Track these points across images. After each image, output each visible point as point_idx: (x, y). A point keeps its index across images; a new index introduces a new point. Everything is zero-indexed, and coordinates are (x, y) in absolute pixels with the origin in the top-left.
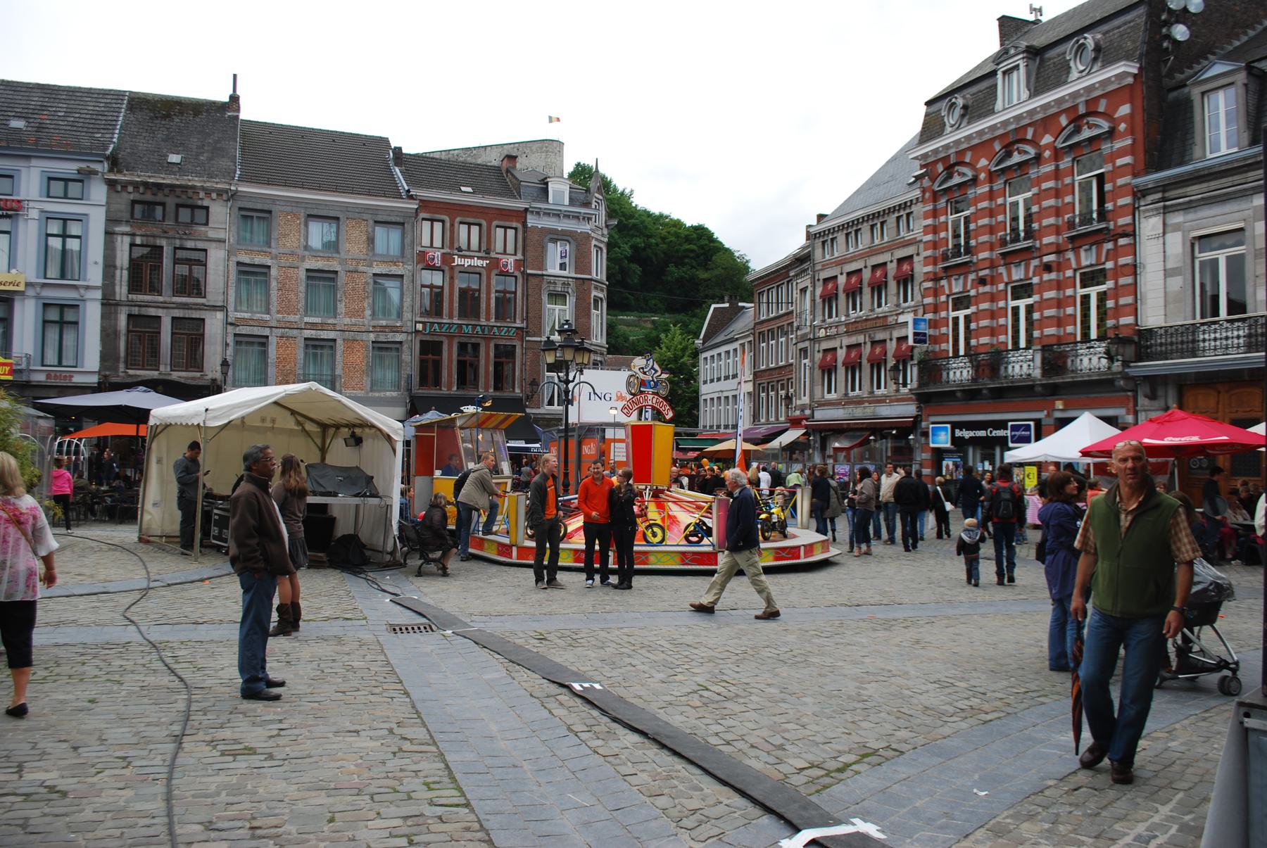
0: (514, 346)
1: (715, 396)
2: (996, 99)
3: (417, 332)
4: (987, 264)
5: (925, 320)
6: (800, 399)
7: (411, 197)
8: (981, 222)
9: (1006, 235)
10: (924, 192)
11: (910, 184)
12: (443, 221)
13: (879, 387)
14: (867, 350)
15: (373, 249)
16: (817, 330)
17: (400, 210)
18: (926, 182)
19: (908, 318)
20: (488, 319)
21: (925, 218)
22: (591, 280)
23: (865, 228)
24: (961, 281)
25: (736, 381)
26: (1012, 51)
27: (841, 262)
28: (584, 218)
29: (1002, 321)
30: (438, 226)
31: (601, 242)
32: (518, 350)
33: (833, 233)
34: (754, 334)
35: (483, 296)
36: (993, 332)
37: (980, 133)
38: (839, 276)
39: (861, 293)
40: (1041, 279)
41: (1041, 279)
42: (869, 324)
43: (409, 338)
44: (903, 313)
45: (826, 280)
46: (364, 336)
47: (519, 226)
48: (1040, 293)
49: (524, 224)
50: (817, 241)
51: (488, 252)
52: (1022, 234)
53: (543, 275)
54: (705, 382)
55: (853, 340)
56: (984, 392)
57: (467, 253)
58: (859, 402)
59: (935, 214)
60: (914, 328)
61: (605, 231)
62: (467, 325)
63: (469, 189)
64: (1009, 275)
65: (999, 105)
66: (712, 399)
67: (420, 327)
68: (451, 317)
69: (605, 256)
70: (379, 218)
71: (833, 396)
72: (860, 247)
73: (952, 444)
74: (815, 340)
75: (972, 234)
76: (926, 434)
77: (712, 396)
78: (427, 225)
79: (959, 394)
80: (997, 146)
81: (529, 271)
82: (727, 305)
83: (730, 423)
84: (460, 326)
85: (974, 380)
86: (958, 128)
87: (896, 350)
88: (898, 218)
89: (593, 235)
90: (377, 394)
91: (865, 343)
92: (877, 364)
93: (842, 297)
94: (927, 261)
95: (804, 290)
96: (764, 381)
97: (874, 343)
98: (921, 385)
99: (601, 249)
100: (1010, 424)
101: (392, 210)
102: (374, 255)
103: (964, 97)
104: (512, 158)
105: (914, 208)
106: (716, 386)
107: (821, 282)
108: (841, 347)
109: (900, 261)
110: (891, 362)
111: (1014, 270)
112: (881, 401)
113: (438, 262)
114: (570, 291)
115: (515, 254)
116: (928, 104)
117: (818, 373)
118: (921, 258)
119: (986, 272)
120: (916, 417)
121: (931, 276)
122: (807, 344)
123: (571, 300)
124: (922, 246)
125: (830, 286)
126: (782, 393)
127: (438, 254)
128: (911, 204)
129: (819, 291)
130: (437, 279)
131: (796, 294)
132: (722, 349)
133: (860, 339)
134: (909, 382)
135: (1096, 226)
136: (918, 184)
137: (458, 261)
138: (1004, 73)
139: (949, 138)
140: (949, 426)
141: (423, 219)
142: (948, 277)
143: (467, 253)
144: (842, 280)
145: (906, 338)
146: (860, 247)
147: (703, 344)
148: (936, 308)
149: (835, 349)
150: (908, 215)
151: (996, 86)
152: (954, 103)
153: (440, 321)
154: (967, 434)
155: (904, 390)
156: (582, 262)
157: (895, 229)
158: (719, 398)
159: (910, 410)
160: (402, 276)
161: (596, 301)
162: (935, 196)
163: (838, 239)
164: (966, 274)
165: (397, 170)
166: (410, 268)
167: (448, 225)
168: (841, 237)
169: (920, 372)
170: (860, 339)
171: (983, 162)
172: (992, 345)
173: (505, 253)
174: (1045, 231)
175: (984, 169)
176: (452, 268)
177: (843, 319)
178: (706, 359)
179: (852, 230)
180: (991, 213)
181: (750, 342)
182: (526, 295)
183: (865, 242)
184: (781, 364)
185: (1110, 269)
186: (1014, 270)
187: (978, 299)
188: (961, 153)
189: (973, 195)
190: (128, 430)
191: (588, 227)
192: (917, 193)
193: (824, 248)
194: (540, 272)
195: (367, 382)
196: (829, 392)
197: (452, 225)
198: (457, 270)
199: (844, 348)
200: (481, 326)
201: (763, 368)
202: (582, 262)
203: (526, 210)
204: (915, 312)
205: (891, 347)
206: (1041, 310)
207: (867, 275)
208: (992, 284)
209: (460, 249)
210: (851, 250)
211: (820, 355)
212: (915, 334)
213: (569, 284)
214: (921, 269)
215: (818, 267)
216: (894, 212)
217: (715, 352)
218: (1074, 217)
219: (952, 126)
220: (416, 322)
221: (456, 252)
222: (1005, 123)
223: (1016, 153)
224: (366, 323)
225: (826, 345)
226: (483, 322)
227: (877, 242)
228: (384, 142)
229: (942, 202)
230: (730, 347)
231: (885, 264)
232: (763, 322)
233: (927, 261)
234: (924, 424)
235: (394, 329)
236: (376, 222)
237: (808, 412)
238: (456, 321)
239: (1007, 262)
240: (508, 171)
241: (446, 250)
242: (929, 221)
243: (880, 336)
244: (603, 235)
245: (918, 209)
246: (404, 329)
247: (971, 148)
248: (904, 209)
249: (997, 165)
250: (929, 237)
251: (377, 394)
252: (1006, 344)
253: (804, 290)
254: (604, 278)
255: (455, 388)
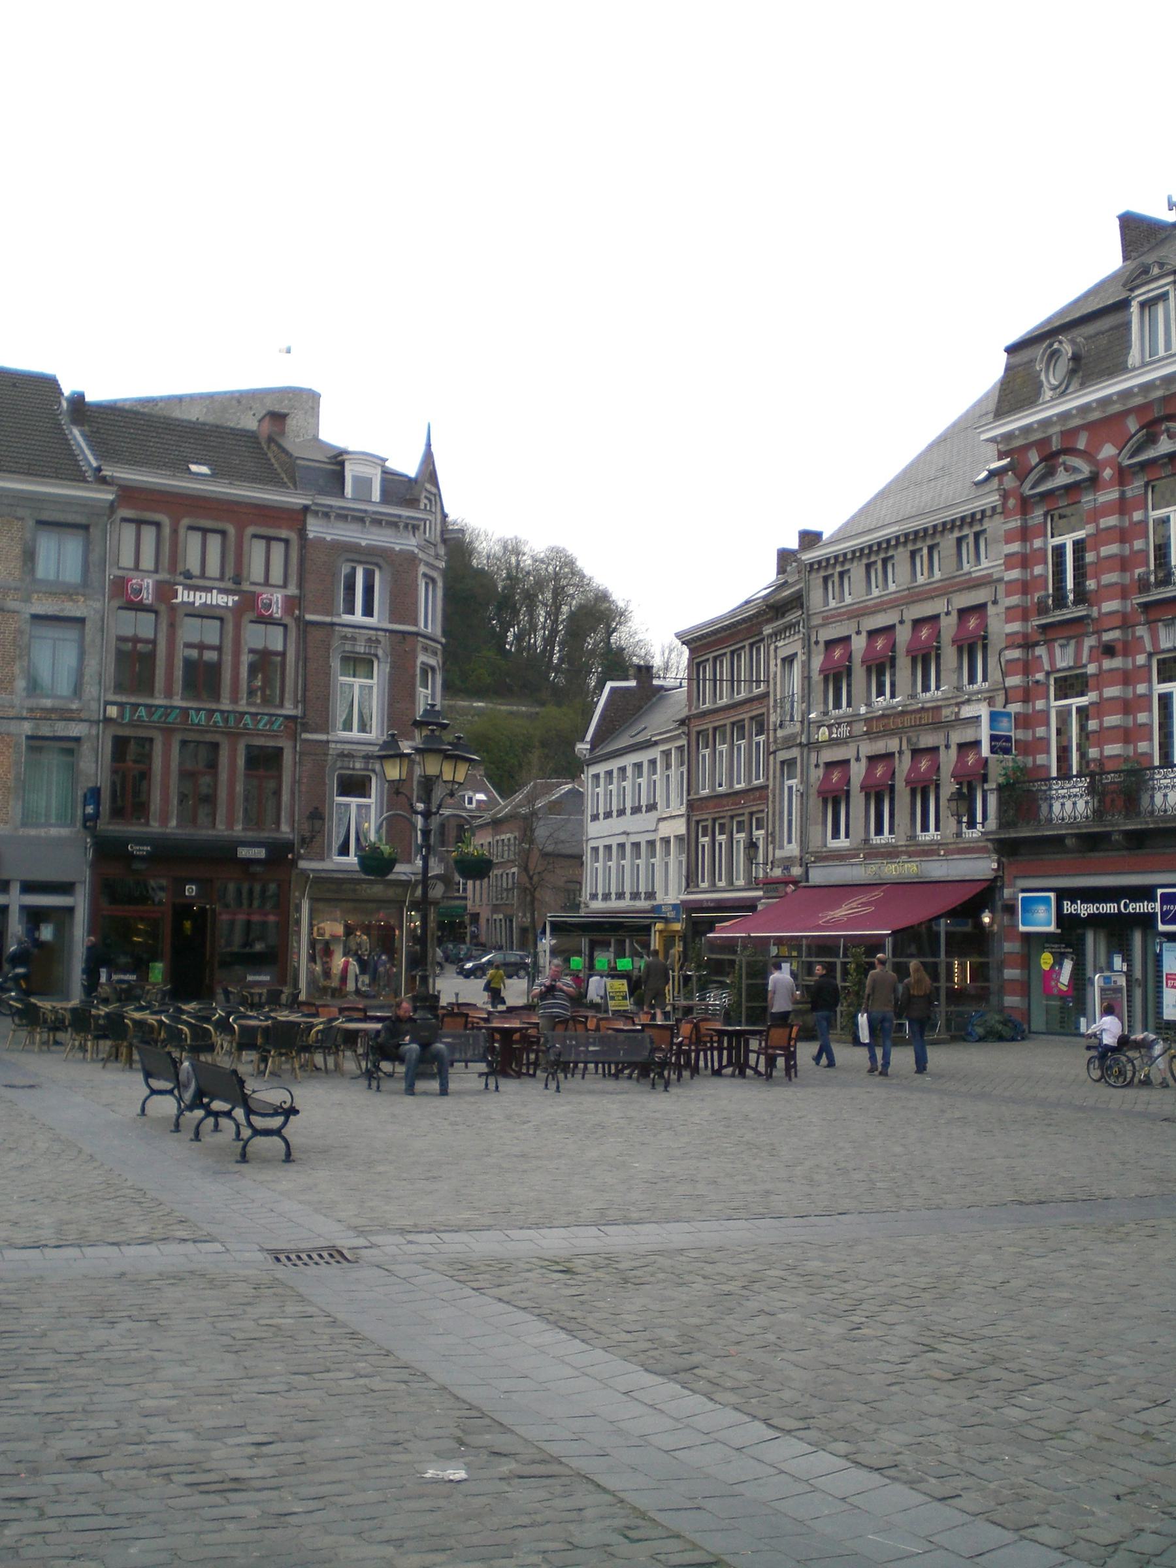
0: (281, 749)
1: (614, 842)
2: (1130, 347)
3: (108, 720)
4: (1117, 621)
5: (1008, 715)
6: (781, 847)
7: (103, 481)
8: (1105, 551)
9: (1148, 573)
10: (1005, 496)
11: (978, 484)
12: (158, 525)
13: (925, 828)
14: (904, 765)
15: (33, 571)
16: (813, 728)
17: (84, 503)
18: (1010, 481)
19: (982, 710)
20: (235, 700)
21: (1008, 541)
22: (417, 634)
23: (901, 555)
24: (1071, 650)
25: (654, 815)
26: (1156, 271)
27: (857, 613)
28: (406, 526)
29: (1142, 718)
30: (149, 534)
31: (434, 567)
32: (288, 758)
33: (843, 563)
34: (688, 735)
35: (228, 658)
36: (1127, 735)
37: (1104, 402)
38: (854, 637)
39: (893, 666)
40: (1100, 667)
41: (1100, 667)
42: (907, 721)
43: (94, 732)
44: (968, 701)
45: (830, 644)
46: (13, 727)
47: (293, 536)
48: (1099, 688)
49: (302, 532)
50: (814, 575)
51: (237, 580)
52: (1071, 597)
53: (333, 624)
54: (595, 817)
55: (880, 747)
56: (1115, 837)
57: (201, 582)
58: (891, 853)
59: (1024, 534)
60: (992, 728)
61: (442, 551)
62: (198, 710)
63: (204, 469)
64: (1155, 639)
65: (1134, 357)
66: (608, 848)
67: (113, 711)
68: (169, 694)
69: (440, 593)
70: (45, 516)
71: (843, 843)
72: (892, 587)
73: (1058, 926)
74: (812, 746)
75: (1090, 570)
76: (1010, 909)
77: (607, 842)
78: (129, 531)
79: (1069, 842)
80: (1132, 425)
81: (309, 617)
82: (632, 683)
83: (642, 889)
84: (185, 711)
85: (1099, 814)
86: (1063, 394)
87: (911, 770)
88: (959, 540)
89: (421, 555)
90: (33, 832)
91: (900, 752)
92: (922, 789)
93: (859, 672)
94: (1011, 614)
95: (789, 660)
96: (706, 815)
97: (916, 753)
98: (1003, 825)
99: (433, 580)
100: (1160, 891)
101: (69, 502)
102: (35, 581)
103: (1073, 342)
104: (278, 418)
105: (987, 524)
106: (616, 824)
107: (822, 646)
108: (858, 759)
109: (964, 613)
110: (949, 787)
111: (1162, 632)
112: (928, 851)
113: (148, 597)
114: (380, 653)
115: (285, 586)
116: (1011, 350)
117: (815, 802)
118: (1000, 608)
119: (1115, 635)
120: (995, 879)
121: (1020, 640)
122: (795, 752)
123: (381, 671)
124: (1001, 588)
125: (837, 653)
126: (741, 836)
127: (149, 582)
128: (934, 533)
129: (817, 662)
130: (144, 626)
131: (775, 668)
132: (629, 760)
133: (893, 745)
134: (979, 819)
135: (1072, 612)
136: (995, 482)
137: (183, 596)
138: (1143, 305)
139: (1048, 410)
140: (1052, 895)
141: (125, 520)
142: (1049, 642)
143: (201, 582)
144: (859, 644)
145: (977, 744)
146: (892, 587)
147: (592, 749)
148: (1027, 695)
149: (847, 762)
150: (977, 536)
151: (1127, 325)
152: (1057, 351)
153: (149, 701)
154: (1084, 909)
155: (975, 834)
156: (402, 607)
157: (955, 559)
158: (622, 846)
159: (984, 867)
160: (81, 621)
161: (424, 673)
162: (1025, 505)
163: (853, 573)
164: (1079, 639)
165: (76, 432)
166: (97, 605)
167: (167, 531)
168: (857, 571)
169: (1001, 803)
170: (893, 745)
171: (1108, 451)
172: (1127, 759)
173: (267, 583)
174: (1105, 592)
175: (1109, 462)
176: (173, 609)
177: (863, 710)
178: (596, 777)
179: (878, 559)
180: (1123, 536)
181: (680, 749)
182: (304, 658)
183: (898, 579)
184: (737, 787)
185: (1093, 675)
186: (1162, 632)
187: (1101, 679)
188: (1070, 434)
189: (1091, 505)
190: (278, 701)
191: (414, 542)
192: (994, 499)
193: (826, 588)
194: (328, 619)
195: (15, 809)
196: (836, 835)
197: (175, 531)
198: (181, 612)
199: (864, 761)
200: (222, 712)
201: (705, 792)
202: (402, 607)
203: (306, 509)
204: (991, 701)
205: (948, 759)
206: (1100, 716)
207: (903, 635)
208: (1126, 654)
209: (188, 575)
210: (876, 592)
211: (821, 772)
212: (993, 738)
213: (378, 641)
214: (1000, 627)
215: (816, 621)
216: (952, 529)
217: (614, 765)
218: (1148, 573)
219: (1054, 389)
220: (107, 703)
221: (181, 579)
222: (1147, 387)
223: (1164, 437)
224: (17, 701)
225: (829, 755)
226: (226, 705)
227: (921, 580)
228: (48, 384)
229: (1038, 513)
230: (643, 757)
231: (936, 617)
232: (704, 714)
233: (1011, 614)
234: (1007, 892)
235: (67, 716)
236: (41, 523)
237: (796, 871)
238: (178, 702)
239: (1152, 618)
240: (271, 440)
241: (163, 576)
242: (1015, 547)
243: (927, 740)
244: (437, 557)
245: (996, 526)
246: (83, 715)
247: (1089, 427)
248: (971, 525)
249: (1131, 457)
250: (1015, 574)
251: (33, 832)
252: (1150, 756)
253: (789, 660)
254: (438, 632)
255: (174, 823)
